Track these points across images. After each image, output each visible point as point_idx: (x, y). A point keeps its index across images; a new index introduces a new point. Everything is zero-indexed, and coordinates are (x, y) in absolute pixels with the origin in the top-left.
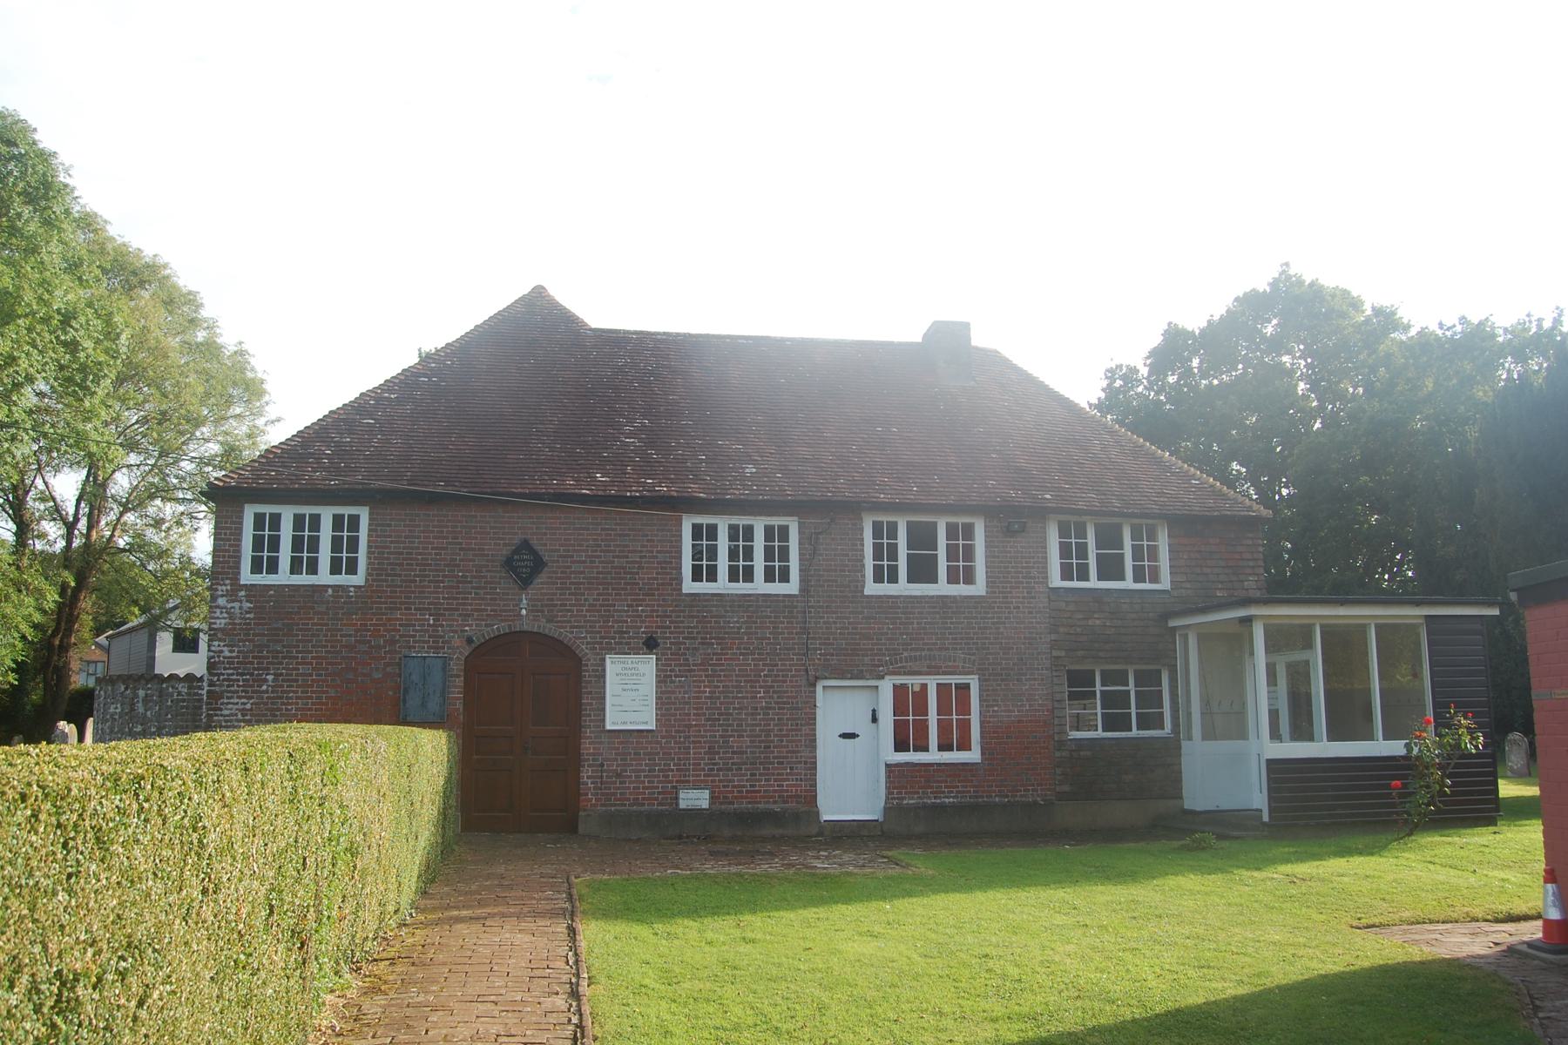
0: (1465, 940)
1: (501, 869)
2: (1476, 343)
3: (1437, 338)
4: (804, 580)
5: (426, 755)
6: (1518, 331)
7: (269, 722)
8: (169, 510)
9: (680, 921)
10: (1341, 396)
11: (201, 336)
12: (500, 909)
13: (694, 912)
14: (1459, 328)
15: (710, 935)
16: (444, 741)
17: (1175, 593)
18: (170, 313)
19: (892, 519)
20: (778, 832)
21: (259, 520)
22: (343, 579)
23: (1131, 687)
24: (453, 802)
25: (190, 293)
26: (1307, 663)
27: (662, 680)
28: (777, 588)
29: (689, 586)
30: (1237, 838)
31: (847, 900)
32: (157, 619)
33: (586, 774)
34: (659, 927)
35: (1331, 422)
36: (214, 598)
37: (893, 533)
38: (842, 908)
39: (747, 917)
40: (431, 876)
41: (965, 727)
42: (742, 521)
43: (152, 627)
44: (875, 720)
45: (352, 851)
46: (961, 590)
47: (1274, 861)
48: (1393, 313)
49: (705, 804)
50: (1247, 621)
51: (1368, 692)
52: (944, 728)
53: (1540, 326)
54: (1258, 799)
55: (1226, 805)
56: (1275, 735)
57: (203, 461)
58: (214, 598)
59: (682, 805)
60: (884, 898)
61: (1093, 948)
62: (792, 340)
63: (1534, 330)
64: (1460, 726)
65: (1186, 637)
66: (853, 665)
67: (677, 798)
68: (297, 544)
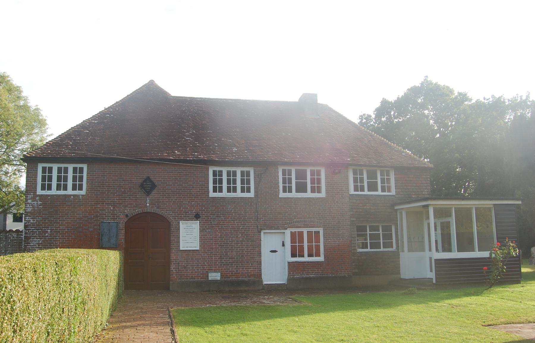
0: (531, 331)
1: (141, 305)
2: (497, 106)
3: (484, 103)
4: (256, 192)
5: (112, 260)
6: (514, 100)
7: (48, 248)
8: (11, 169)
9: (215, 326)
10: (446, 126)
11: (22, 103)
12: (142, 322)
13: (220, 322)
14: (491, 100)
15: (228, 332)
16: (118, 255)
17: (397, 196)
18: (10, 94)
19: (289, 168)
20: (247, 288)
21: (44, 169)
22: (77, 192)
23: (381, 232)
24: (121, 279)
25: (18, 87)
26: (449, 222)
27: (202, 230)
28: (246, 195)
29: (212, 194)
30: (423, 289)
31: (280, 316)
32: (7, 209)
33: (173, 267)
34: (207, 329)
35: (443, 134)
36: (27, 200)
37: (290, 174)
38: (279, 319)
39: (242, 325)
40: (114, 309)
41: (318, 247)
42: (232, 169)
43: (5, 213)
44: (283, 245)
45: (84, 303)
46: (316, 195)
47: (442, 299)
48: (466, 95)
49: (219, 278)
50: (427, 206)
51: (472, 233)
52: (310, 248)
53: (521, 98)
54: (432, 275)
55: (417, 276)
56: (437, 250)
57: (22, 150)
58: (27, 200)
59: (210, 278)
60: (294, 316)
61: (385, 336)
62: (249, 101)
63: (519, 100)
64: (510, 246)
65: (401, 213)
66: (274, 225)
67: (208, 276)
68: (59, 179)
